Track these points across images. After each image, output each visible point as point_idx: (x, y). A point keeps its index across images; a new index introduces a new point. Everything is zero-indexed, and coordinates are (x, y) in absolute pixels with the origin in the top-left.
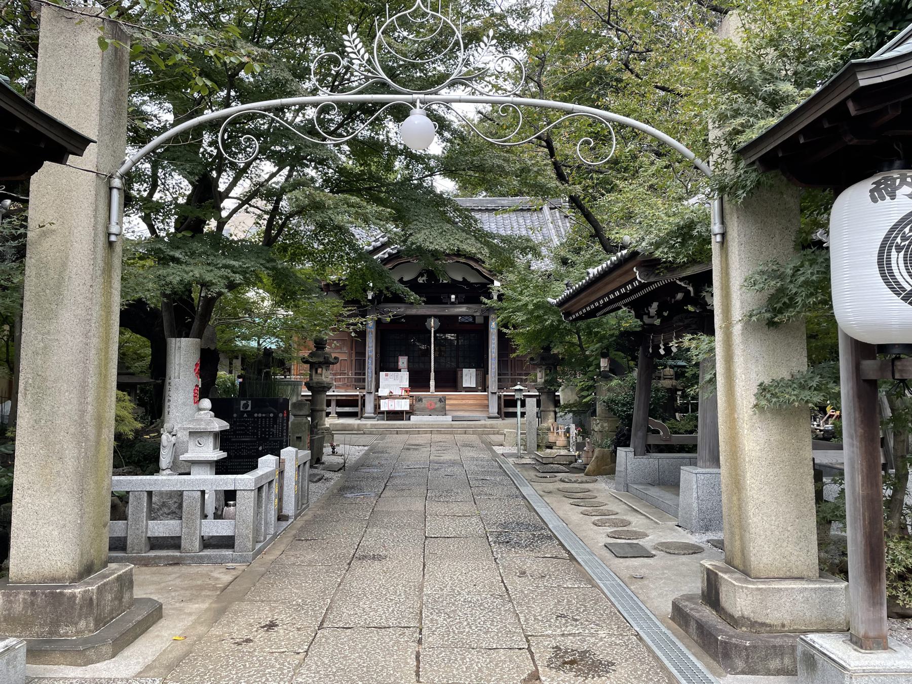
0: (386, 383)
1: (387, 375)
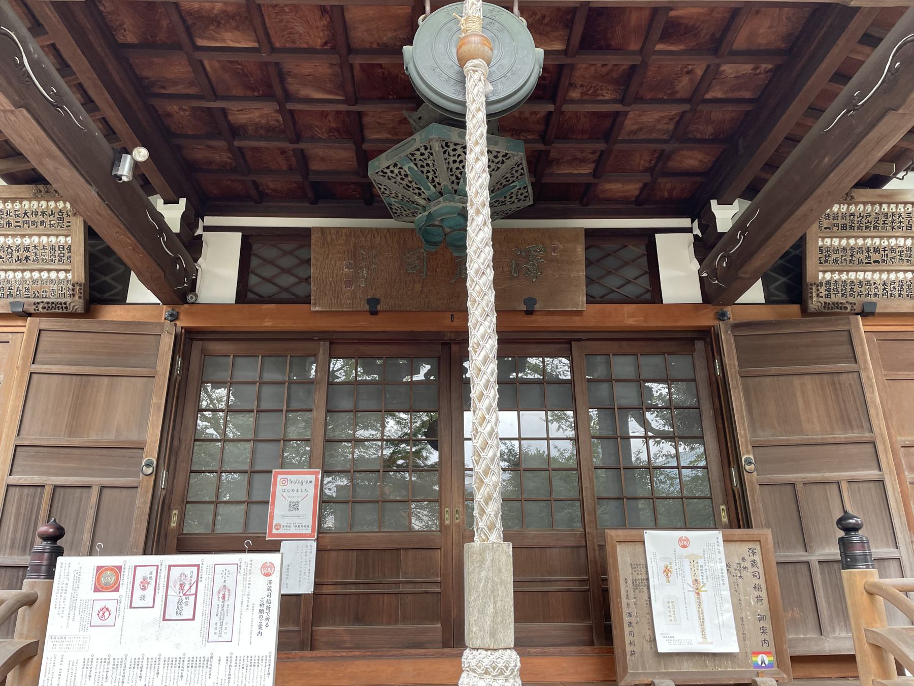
0: (103, 642)
1: (106, 582)
